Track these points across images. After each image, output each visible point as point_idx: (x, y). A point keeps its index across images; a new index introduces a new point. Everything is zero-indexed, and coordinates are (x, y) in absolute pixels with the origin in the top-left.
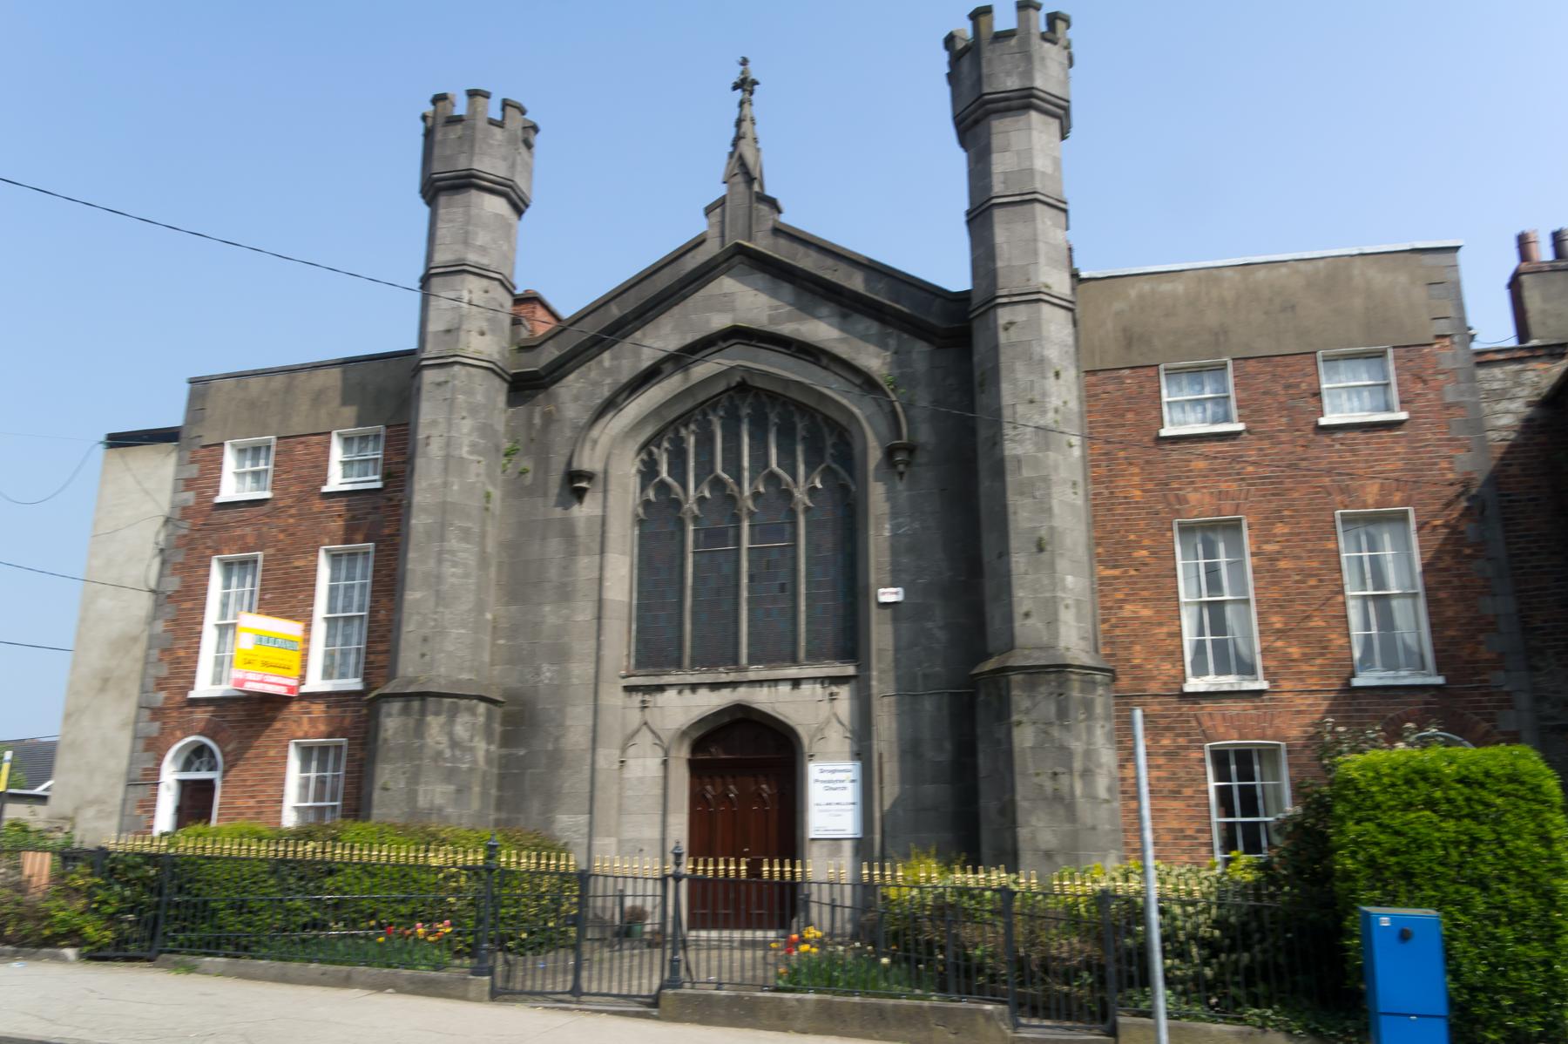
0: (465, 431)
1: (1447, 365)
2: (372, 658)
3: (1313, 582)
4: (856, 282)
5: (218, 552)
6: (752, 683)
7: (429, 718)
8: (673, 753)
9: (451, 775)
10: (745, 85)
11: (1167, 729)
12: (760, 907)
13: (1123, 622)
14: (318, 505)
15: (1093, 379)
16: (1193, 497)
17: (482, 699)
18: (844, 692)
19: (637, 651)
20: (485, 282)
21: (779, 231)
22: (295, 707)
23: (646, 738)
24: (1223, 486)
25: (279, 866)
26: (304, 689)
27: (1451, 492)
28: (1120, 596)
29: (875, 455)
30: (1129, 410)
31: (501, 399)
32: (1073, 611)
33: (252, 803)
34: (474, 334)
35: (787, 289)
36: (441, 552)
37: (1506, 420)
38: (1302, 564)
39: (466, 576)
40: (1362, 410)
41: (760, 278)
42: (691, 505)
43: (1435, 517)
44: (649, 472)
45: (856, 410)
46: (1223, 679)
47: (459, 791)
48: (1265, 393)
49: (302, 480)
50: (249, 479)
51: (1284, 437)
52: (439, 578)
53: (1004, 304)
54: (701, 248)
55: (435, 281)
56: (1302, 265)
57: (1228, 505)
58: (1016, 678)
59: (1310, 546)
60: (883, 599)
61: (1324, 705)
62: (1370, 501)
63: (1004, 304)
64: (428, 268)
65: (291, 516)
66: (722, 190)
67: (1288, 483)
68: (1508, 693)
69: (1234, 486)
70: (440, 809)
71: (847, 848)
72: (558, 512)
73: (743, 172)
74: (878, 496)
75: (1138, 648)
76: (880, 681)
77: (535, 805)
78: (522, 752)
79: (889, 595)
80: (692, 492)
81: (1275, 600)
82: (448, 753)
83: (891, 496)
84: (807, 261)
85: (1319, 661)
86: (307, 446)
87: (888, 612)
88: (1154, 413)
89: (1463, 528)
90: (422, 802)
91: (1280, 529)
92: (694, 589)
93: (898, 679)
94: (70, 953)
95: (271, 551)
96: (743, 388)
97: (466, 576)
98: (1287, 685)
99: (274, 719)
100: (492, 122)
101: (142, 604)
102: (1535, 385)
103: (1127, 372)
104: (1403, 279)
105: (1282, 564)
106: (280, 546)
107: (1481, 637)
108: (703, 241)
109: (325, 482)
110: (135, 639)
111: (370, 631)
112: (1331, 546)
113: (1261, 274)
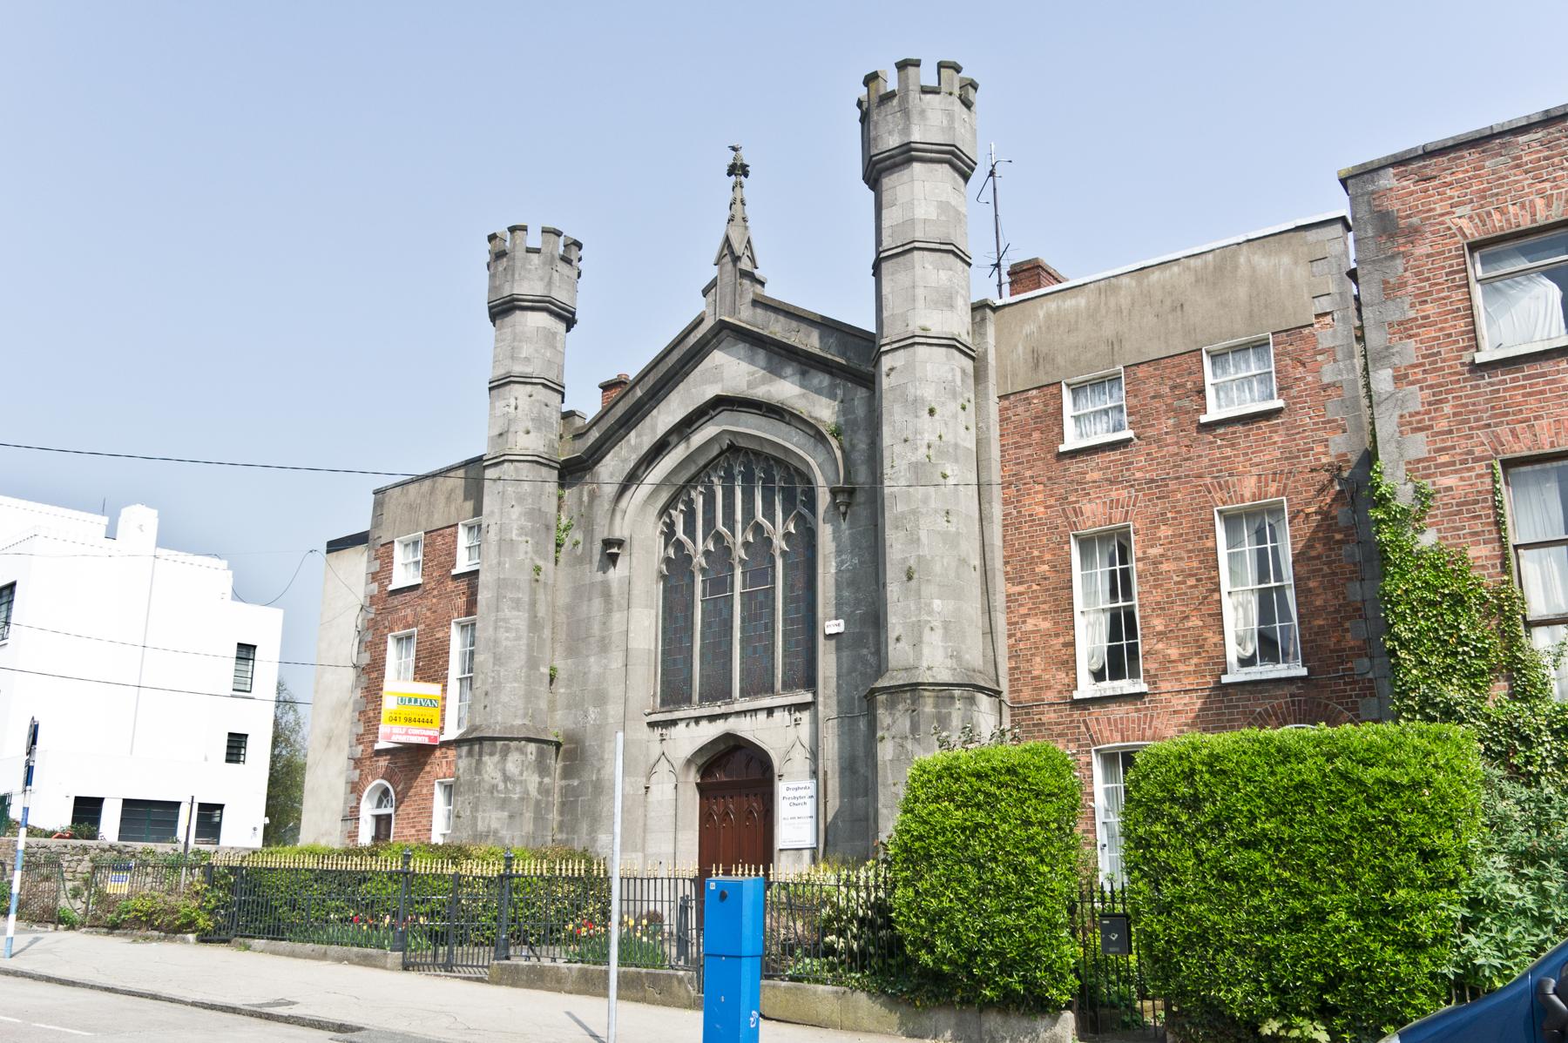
0: (514, 517)
1: (1325, 343)
4: (811, 341)
5: (391, 630)
6: (738, 713)
7: (486, 758)
9: (504, 803)
10: (738, 169)
11: (1059, 735)
13: (1026, 636)
14: (451, 585)
15: (1006, 403)
16: (1088, 508)
17: (529, 740)
18: (805, 716)
19: (662, 691)
20: (529, 387)
21: (759, 303)
22: (438, 753)
23: (663, 764)
24: (1114, 495)
25: (321, 876)
26: (443, 738)
27: (1324, 477)
28: (1023, 611)
29: (823, 499)
30: (1036, 429)
31: (552, 487)
32: (939, 632)
33: (413, 831)
34: (521, 433)
35: (761, 355)
36: (496, 621)
38: (1183, 565)
39: (518, 638)
40: (1253, 400)
41: (742, 348)
42: (699, 560)
43: (1308, 504)
45: (809, 459)
47: (511, 817)
48: (1153, 397)
49: (441, 566)
50: (412, 567)
51: (1169, 439)
52: (496, 642)
53: (887, 352)
54: (1498, 224)
55: (885, 266)
56: (1192, 261)
58: (881, 698)
59: (1190, 547)
60: (828, 631)
61: (1199, 704)
62: (1247, 495)
63: (887, 352)
64: (878, 253)
66: (714, 272)
67: (1172, 485)
68: (1370, 680)
70: (496, 832)
71: (807, 855)
72: (599, 576)
74: (825, 533)
75: (1038, 659)
76: (825, 706)
77: (584, 827)
78: (576, 783)
79: (834, 626)
80: (699, 547)
81: (1158, 603)
82: (501, 786)
83: (837, 536)
85: (1195, 660)
87: (833, 642)
88: (1056, 430)
89: (1334, 513)
90: (481, 827)
91: (1164, 531)
92: (702, 634)
93: (839, 703)
94: (191, 937)
95: (422, 627)
96: (733, 448)
97: (518, 638)
99: (425, 764)
100: (925, 91)
101: (351, 674)
103: (1034, 392)
104: (1286, 260)
107: (1347, 625)
109: (454, 566)
110: (346, 705)
112: (1210, 544)
113: (1155, 276)
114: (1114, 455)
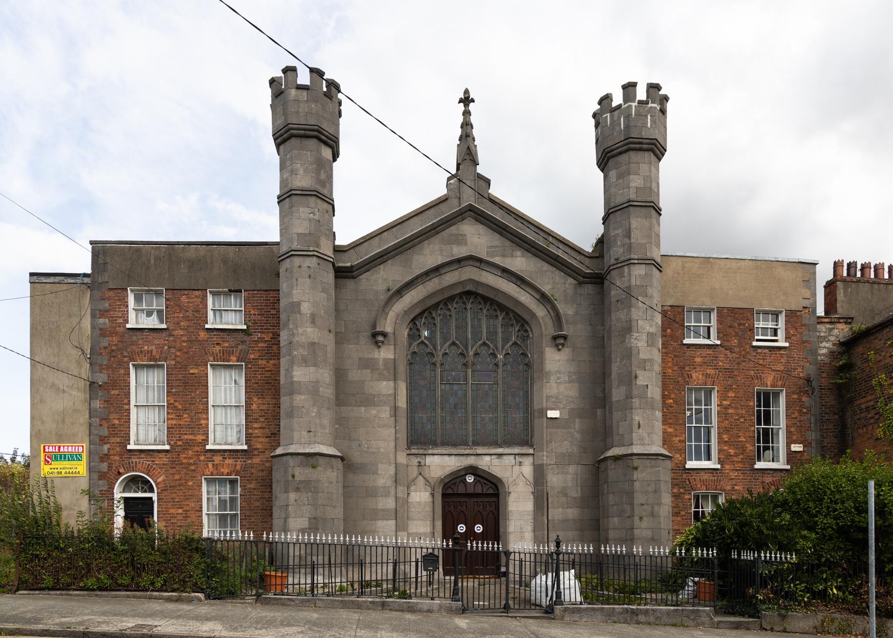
2: (250, 431)
3: (742, 420)
5: (132, 359)
8: (436, 490)
10: (466, 100)
12: (460, 565)
24: (708, 371)
33: (180, 511)
37: (824, 351)
44: (414, 334)
46: (698, 462)
48: (730, 327)
57: (709, 380)
60: (549, 416)
65: (183, 341)
67: (736, 373)
69: (713, 372)
73: (467, 154)
84: (498, 215)
85: (741, 456)
86: (188, 298)
91: (731, 394)
98: (727, 467)
102: (837, 337)
105: (730, 411)
106: (178, 359)
108: (447, 199)
111: (247, 416)
114: (710, 352)
